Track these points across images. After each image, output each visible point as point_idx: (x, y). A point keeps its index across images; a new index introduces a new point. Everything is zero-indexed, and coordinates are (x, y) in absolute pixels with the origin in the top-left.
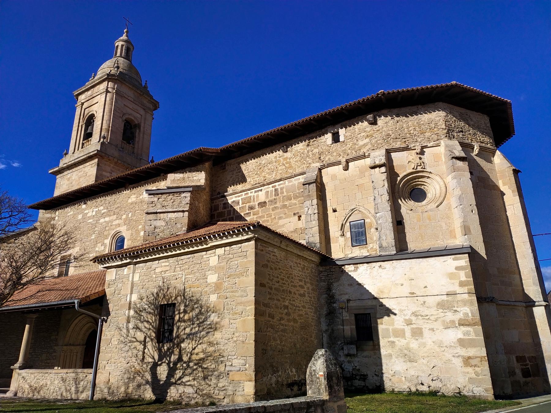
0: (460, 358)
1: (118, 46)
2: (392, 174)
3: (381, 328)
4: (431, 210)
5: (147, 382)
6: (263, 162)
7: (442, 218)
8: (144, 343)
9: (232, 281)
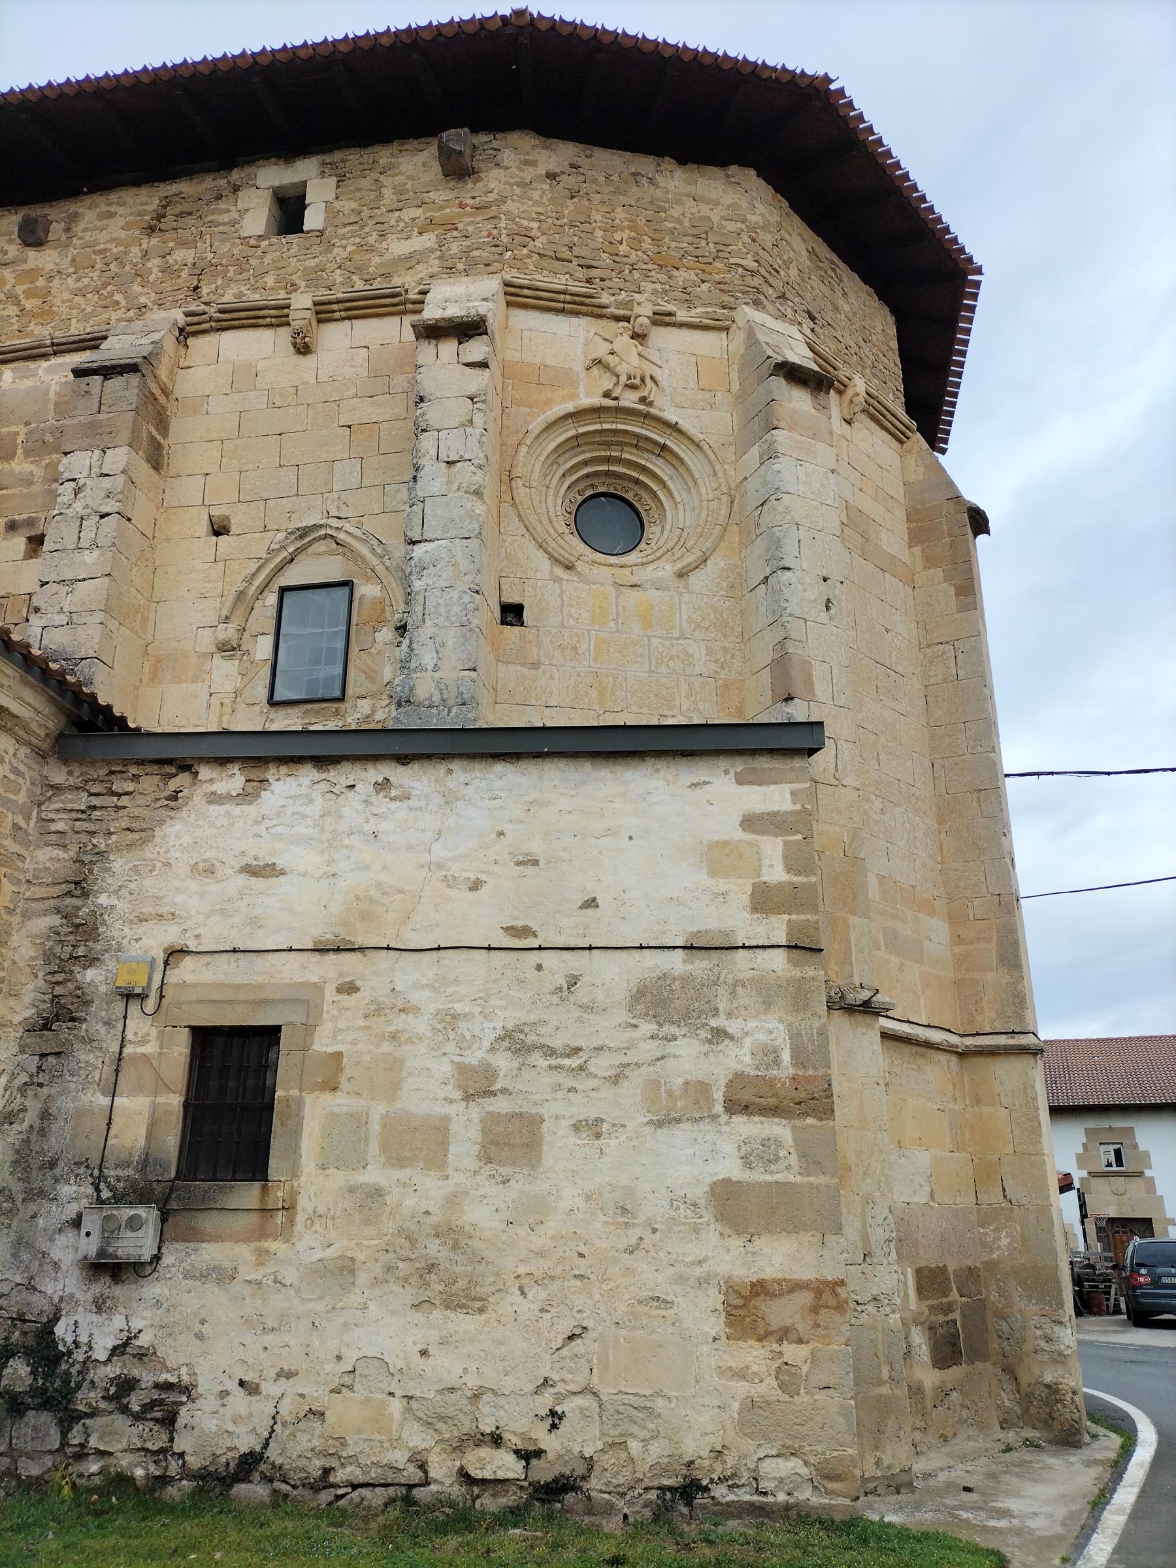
0: (713, 1291)
7: (698, 626)
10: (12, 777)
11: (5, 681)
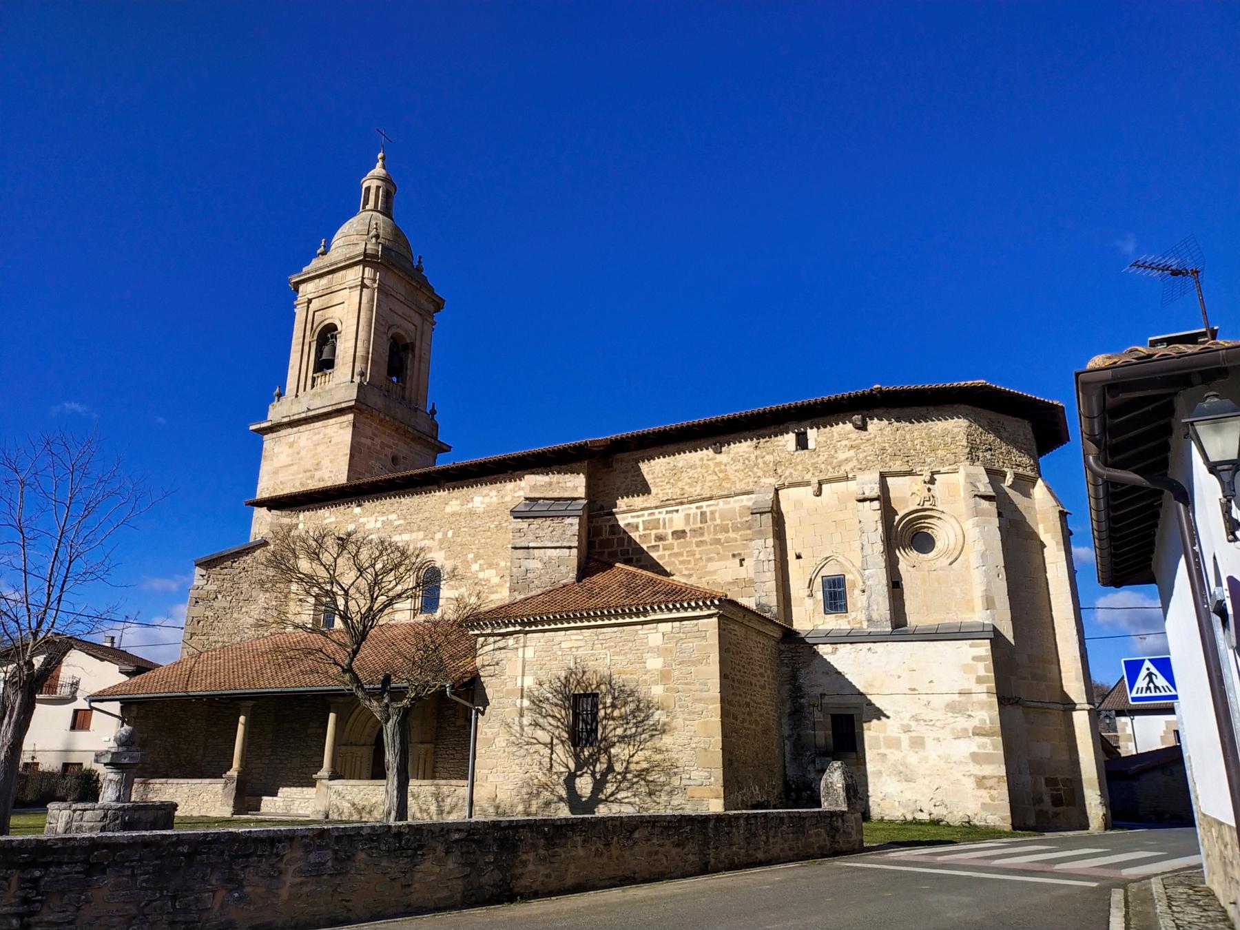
1: (368, 189)
2: (888, 511)
3: (867, 735)
4: (942, 569)
5: (561, 799)
6: (680, 465)
8: (551, 746)
9: (684, 669)
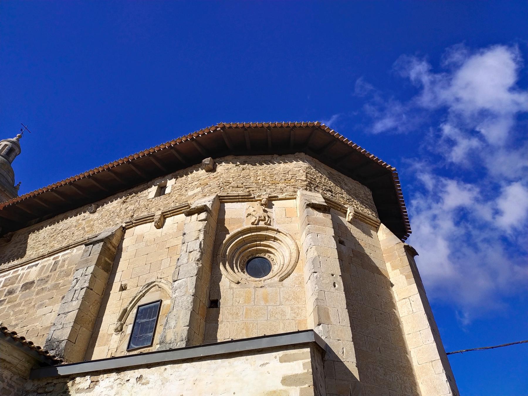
4: (270, 286)
7: (287, 300)
10: (8, 388)
11: (3, 348)
